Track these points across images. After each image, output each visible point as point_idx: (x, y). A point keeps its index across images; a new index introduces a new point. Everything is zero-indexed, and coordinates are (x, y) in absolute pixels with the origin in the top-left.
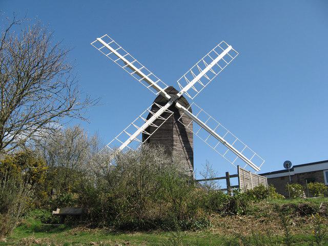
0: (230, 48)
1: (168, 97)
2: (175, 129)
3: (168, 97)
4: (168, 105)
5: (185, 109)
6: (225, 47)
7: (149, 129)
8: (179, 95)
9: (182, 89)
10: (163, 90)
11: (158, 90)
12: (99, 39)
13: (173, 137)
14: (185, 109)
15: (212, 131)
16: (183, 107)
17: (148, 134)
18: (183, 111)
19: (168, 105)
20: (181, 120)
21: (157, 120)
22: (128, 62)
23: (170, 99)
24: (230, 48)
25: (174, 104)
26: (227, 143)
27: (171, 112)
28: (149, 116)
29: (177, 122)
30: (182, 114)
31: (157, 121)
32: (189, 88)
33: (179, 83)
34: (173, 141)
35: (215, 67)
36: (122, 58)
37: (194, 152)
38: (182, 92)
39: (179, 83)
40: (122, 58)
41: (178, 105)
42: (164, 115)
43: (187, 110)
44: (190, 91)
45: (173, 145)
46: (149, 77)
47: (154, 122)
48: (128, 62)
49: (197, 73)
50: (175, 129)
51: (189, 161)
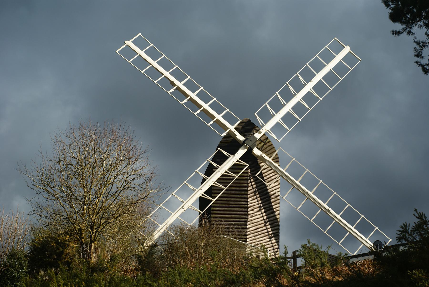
0: (347, 50)
1: (241, 138)
2: (251, 188)
3: (241, 138)
4: (241, 152)
5: (267, 158)
6: (339, 49)
7: (211, 191)
8: (258, 136)
9: (263, 126)
10: (232, 128)
11: (226, 128)
12: (129, 43)
13: (247, 202)
14: (267, 158)
15: (309, 192)
16: (264, 155)
17: (221, 186)
18: (264, 160)
19: (241, 152)
20: (261, 175)
21: (212, 187)
22: (176, 82)
23: (245, 141)
24: (347, 50)
25: (250, 150)
26: (332, 211)
27: (248, 165)
28: (210, 171)
29: (256, 179)
30: (263, 166)
31: (223, 180)
32: (210, 177)
33: (258, 118)
34: (247, 208)
35: (319, 87)
36: (167, 74)
37: (254, 123)
38: (263, 131)
39: (258, 118)
40: (167, 74)
41: (256, 151)
42: (235, 168)
43: (270, 160)
44: (277, 127)
45: (246, 215)
46: (146, 52)
47: (206, 192)
48: (176, 82)
49: (288, 97)
50: (251, 188)
51: (273, 240)
